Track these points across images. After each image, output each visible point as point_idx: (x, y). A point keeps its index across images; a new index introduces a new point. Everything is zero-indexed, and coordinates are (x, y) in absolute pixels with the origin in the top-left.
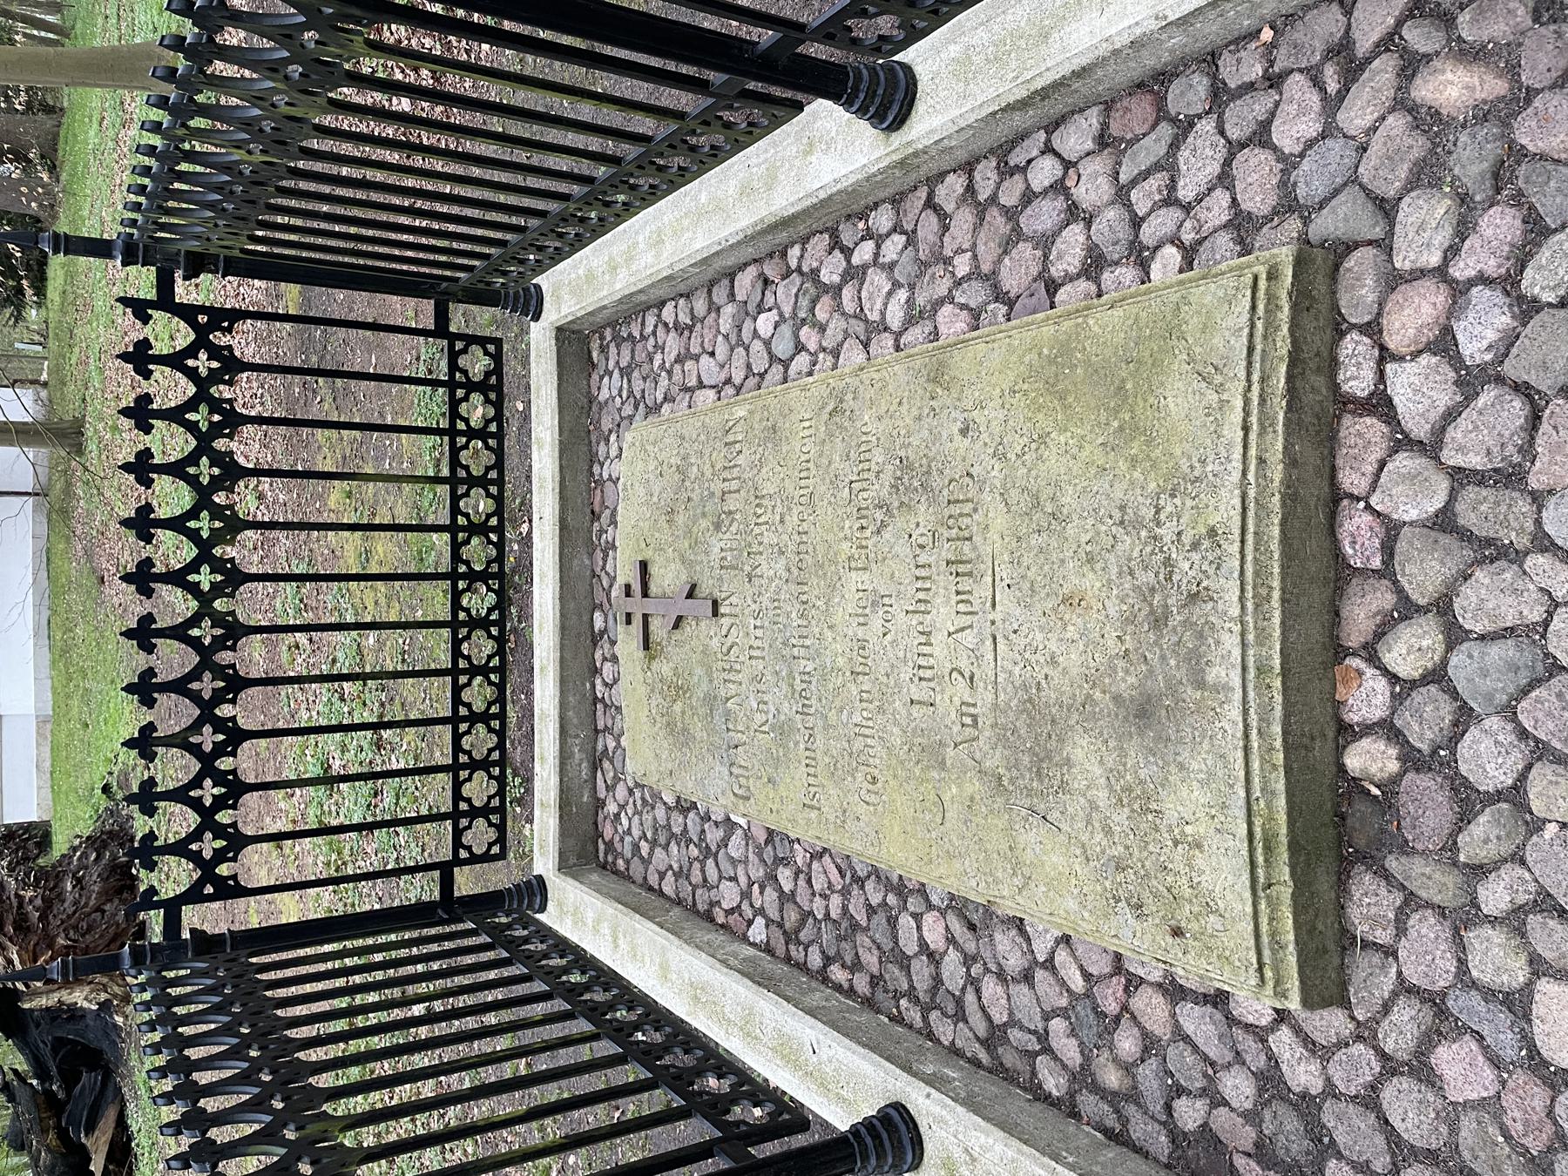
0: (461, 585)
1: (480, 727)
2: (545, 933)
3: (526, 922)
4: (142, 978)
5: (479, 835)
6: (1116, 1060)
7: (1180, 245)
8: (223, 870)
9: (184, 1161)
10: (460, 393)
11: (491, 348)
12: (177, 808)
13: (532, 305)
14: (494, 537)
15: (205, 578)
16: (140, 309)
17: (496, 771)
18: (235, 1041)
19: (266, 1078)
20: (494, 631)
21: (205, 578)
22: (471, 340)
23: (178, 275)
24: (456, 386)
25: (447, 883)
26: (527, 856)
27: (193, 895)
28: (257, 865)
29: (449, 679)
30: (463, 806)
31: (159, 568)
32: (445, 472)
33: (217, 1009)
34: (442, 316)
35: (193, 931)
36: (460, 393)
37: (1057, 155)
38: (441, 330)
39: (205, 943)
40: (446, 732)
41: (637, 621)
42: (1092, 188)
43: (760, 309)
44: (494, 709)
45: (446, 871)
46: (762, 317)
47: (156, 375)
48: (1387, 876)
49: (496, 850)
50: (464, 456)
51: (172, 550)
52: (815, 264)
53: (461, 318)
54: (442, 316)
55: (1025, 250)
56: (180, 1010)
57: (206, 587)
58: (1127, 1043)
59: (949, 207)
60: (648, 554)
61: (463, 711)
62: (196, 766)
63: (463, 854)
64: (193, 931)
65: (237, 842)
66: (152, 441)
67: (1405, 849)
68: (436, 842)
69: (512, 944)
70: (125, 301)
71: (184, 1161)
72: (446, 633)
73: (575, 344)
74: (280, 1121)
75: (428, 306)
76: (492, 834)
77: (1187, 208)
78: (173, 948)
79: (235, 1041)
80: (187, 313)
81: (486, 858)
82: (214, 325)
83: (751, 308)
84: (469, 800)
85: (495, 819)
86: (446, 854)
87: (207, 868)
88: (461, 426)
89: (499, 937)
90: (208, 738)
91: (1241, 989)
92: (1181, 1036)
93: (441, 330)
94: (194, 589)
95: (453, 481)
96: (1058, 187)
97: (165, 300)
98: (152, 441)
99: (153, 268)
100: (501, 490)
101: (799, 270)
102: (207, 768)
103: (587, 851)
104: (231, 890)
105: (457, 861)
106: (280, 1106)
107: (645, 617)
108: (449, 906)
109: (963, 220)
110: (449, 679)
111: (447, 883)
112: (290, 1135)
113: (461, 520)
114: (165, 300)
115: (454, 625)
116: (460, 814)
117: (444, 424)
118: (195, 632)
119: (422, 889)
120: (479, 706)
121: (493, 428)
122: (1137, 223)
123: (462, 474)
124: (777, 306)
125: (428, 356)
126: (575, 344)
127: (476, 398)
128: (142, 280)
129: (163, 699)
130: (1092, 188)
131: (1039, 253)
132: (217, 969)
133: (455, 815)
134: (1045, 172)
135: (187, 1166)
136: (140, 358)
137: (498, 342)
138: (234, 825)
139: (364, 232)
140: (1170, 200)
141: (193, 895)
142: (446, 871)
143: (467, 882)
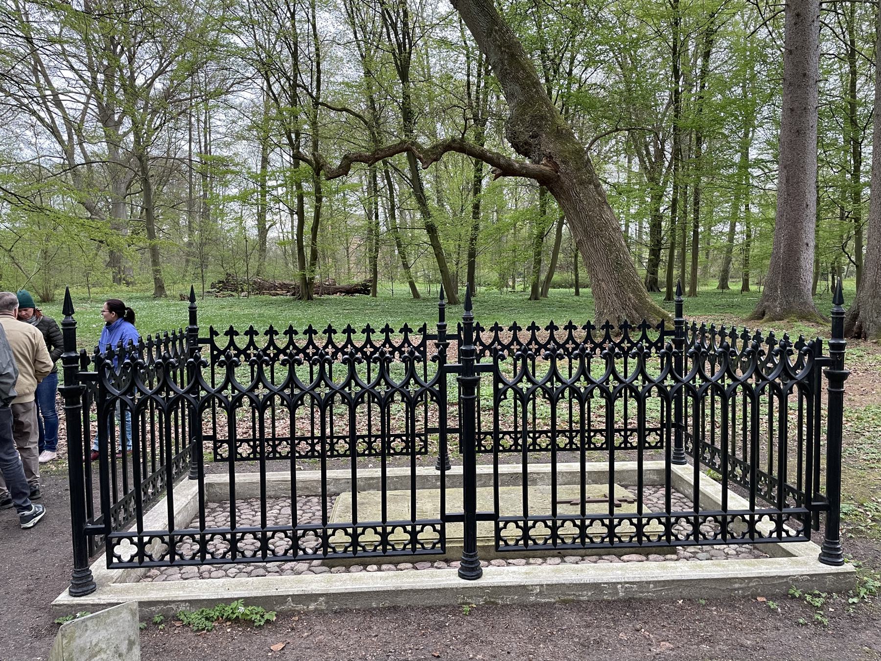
10: (623, 433)
11: (659, 445)
12: (325, 342)
16: (423, 330)
17: (623, 446)
21: (387, 349)
23: (673, 337)
25: (208, 438)
31: (275, 337)
32: (629, 427)
34: (434, 430)
44: (537, 448)
50: (341, 441)
54: (434, 430)
56: (178, 342)
57: (308, 351)
62: (397, 345)
66: (301, 336)
70: (425, 325)
75: (437, 425)
80: (423, 344)
97: (426, 337)
98: (301, 336)
100: (568, 450)
111: (208, 438)
114: (426, 337)
120: (548, 440)
121: (278, 455)
128: (433, 330)
129: (402, 336)
136: (330, 331)
137: (661, 447)
138: (484, 356)
141: (214, 347)
142: (213, 438)
143: (208, 445)
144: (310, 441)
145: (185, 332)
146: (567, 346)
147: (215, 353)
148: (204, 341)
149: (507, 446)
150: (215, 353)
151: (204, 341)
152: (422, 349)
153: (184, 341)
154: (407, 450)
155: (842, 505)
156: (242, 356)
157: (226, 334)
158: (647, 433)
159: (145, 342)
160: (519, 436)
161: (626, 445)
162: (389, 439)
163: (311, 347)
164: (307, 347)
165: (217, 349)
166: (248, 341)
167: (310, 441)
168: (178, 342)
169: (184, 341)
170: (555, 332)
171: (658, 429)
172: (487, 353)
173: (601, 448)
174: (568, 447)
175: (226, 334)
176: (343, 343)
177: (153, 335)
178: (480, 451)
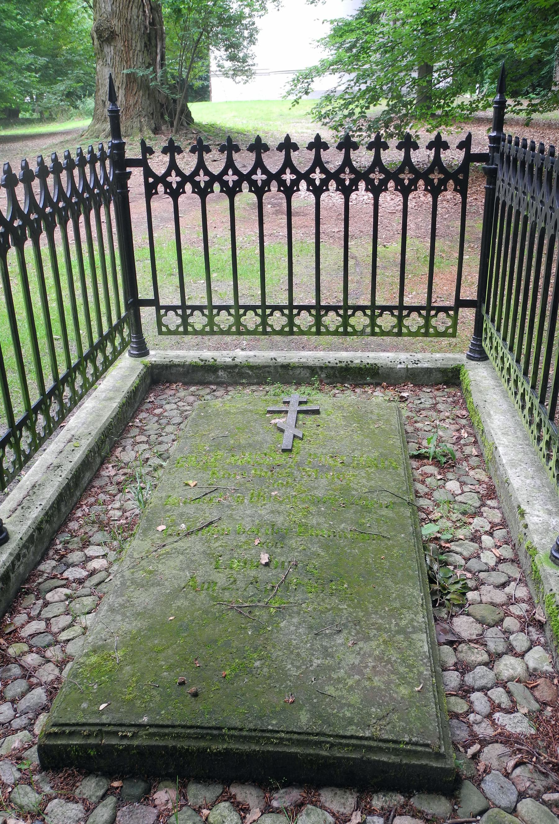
0: (259, 311)
1: (191, 320)
2: (117, 354)
3: (124, 344)
4: (106, 147)
5: (173, 320)
6: (24, 654)
7: (467, 713)
8: (161, 188)
9: (8, 172)
13: (478, 354)
14: (423, 331)
16: (465, 144)
18: (91, 186)
19: (61, 205)
20: (287, 329)
22: (455, 320)
24: (428, 309)
25: (147, 303)
26: (157, 346)
27: (148, 173)
28: (162, 204)
33: (96, 181)
35: (130, 173)
36: (396, 313)
37: (530, 649)
39: (122, 179)
41: (283, 408)
42: (509, 667)
43: (463, 484)
45: (154, 302)
46: (458, 484)
47: (428, 152)
48: (103, 797)
49: (164, 329)
50: (442, 315)
52: (485, 515)
53: (467, 315)
55: (476, 629)
56: (98, 165)
58: (32, 659)
59: (507, 589)
60: (323, 415)
61: (268, 311)
62: (187, 173)
63: (268, 311)
64: (130, 173)
65: (175, 194)
66: (215, 154)
67: (117, 808)
68: (169, 296)
69: (110, 337)
71: (8, 172)
72: (179, 303)
73: (451, 378)
74: (90, 191)
77: (489, 716)
78: (121, 164)
79: (91, 186)
81: (159, 324)
82: (457, 182)
83: (463, 479)
84: (192, 314)
85: (181, 329)
86: (162, 303)
87: (162, 180)
88: (350, 312)
89: (115, 329)
92: (31, 687)
93: (460, 303)
95: (346, 307)
96: (510, 650)
97: (470, 158)
99: (488, 151)
100: (207, 333)
101: (484, 505)
103: (157, 378)
104: (150, 192)
105: (159, 308)
106: (73, 201)
107: (286, 412)
108: (134, 303)
109: (500, 597)
110: (369, 304)
111: (147, 303)
112: (48, 210)
113: (295, 311)
116: (184, 309)
117: (350, 303)
119: (145, 291)
122: (484, 689)
123: (189, 312)
124: (463, 492)
125: (444, 295)
126: (451, 378)
127: (352, 321)
130: (509, 667)
131: (474, 637)
132: (108, 185)
133: (184, 306)
134: (520, 641)
135: (5, 172)
138: (184, 192)
139: (534, 260)
140: (496, 707)
141: (148, 173)
142: (154, 302)
143: (147, 314)
145: (108, 151)
147: (151, 180)
148: (134, 163)
150: (151, 180)
151: (134, 163)
152: (461, 177)
153: (108, 162)
156: (451, 182)
159: (49, 163)
163: (230, 172)
165: (154, 175)
167: (180, 312)
168: (98, 165)
169: (108, 162)
170: (292, 153)
171: (450, 308)
174: (208, 329)
176: (249, 169)
177: (85, 151)
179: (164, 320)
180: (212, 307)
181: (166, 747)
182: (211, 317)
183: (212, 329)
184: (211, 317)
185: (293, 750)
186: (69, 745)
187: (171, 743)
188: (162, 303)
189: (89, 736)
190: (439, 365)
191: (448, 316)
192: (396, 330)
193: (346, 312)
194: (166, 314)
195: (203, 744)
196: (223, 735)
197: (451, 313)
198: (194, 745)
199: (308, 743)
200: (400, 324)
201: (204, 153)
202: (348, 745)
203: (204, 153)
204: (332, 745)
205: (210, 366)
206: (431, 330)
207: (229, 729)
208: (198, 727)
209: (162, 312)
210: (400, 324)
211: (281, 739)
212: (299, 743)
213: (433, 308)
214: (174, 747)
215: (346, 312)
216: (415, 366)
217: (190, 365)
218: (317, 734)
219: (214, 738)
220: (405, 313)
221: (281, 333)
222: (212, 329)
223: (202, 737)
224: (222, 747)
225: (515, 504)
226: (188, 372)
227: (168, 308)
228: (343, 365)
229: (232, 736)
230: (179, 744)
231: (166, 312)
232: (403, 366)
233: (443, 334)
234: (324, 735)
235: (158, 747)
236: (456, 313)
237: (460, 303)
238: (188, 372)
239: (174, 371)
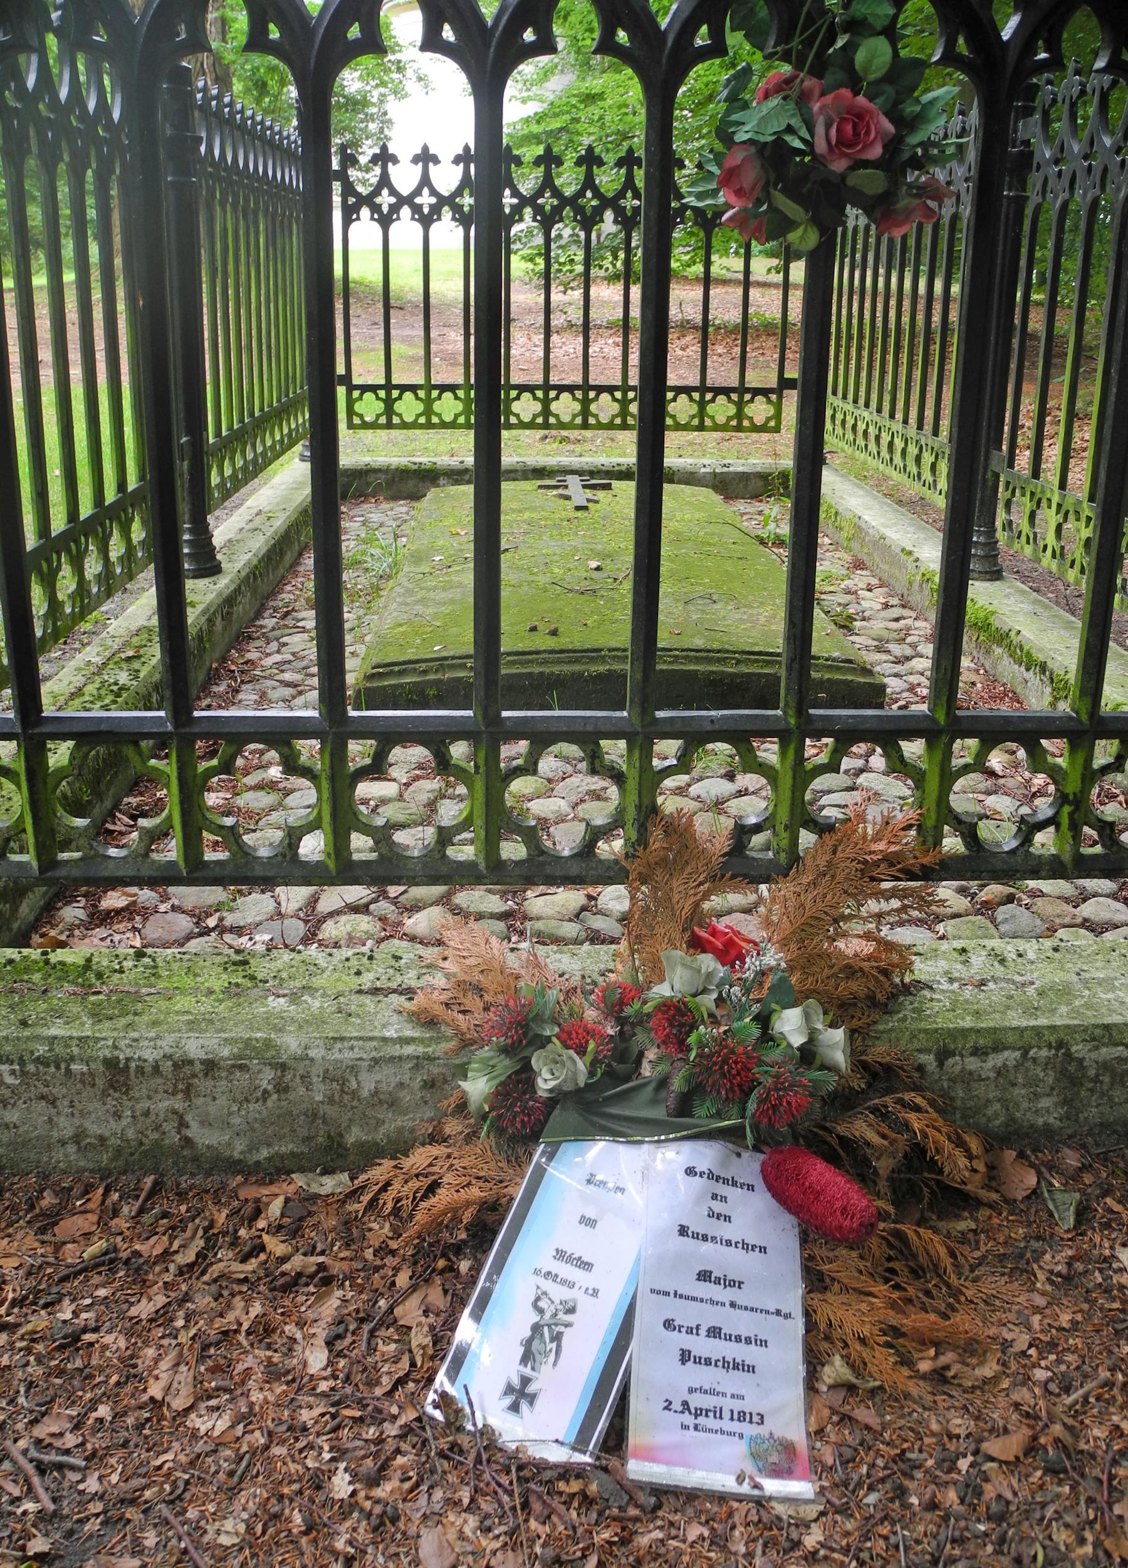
14: (734, 423)
15: (590, 201)
29: (383, 382)
30: (592, 394)
36: (696, 396)
38: (785, 384)
40: (538, 378)
51: (568, 180)
57: (418, 200)
76: (526, 418)
86: (356, 381)
87: (369, 201)
90: (426, 200)
91: (251, 1059)
94: (540, 193)
100: (422, 427)
102: (402, 201)
110: (383, 382)
115: (388, 386)
118: (589, 194)
137: (777, 429)
138: (521, 220)
144: (618, 395)
146: (378, 200)
147: (351, 200)
149: (759, 420)
154: (468, 419)
155: (345, 577)
157: (416, 160)
158: (513, 393)
160: (631, 395)
161: (546, 420)
162: (507, 394)
164: (418, 192)
166: (582, 177)
167: (382, 394)
171: (771, 391)
172: (528, 212)
173: (453, 425)
175: (416, 160)
178: (509, 426)
179: (358, 407)
180: (430, 387)
181: (531, 674)
182: (428, 403)
183: (429, 420)
184: (428, 403)
185: (692, 667)
186: (401, 685)
187: (537, 670)
188: (356, 381)
189: (425, 672)
190: (759, 469)
191: (769, 401)
192: (696, 422)
193: (625, 394)
194: (360, 398)
195: (577, 668)
196: (603, 657)
197: (774, 397)
198: (567, 669)
199: (709, 660)
200: (702, 413)
201: (431, 164)
202: (757, 661)
203: (431, 164)
204: (738, 662)
205: (426, 471)
206: (746, 423)
207: (610, 650)
208: (569, 651)
209: (356, 394)
210: (702, 413)
211: (676, 657)
212: (698, 660)
213: (748, 390)
214: (542, 674)
215: (625, 394)
216: (725, 470)
217: (397, 470)
218: (719, 651)
219: (592, 660)
220: (709, 396)
221: (531, 425)
222: (429, 420)
223: (577, 661)
224: (602, 668)
225: (898, 550)
226: (393, 481)
227: (364, 388)
228: (623, 468)
229: (614, 657)
230: (547, 670)
231: (362, 394)
232: (708, 470)
233: (763, 429)
234: (728, 651)
235: (520, 675)
236: (780, 397)
237: (785, 384)
238: (393, 481)
239: (371, 478)
